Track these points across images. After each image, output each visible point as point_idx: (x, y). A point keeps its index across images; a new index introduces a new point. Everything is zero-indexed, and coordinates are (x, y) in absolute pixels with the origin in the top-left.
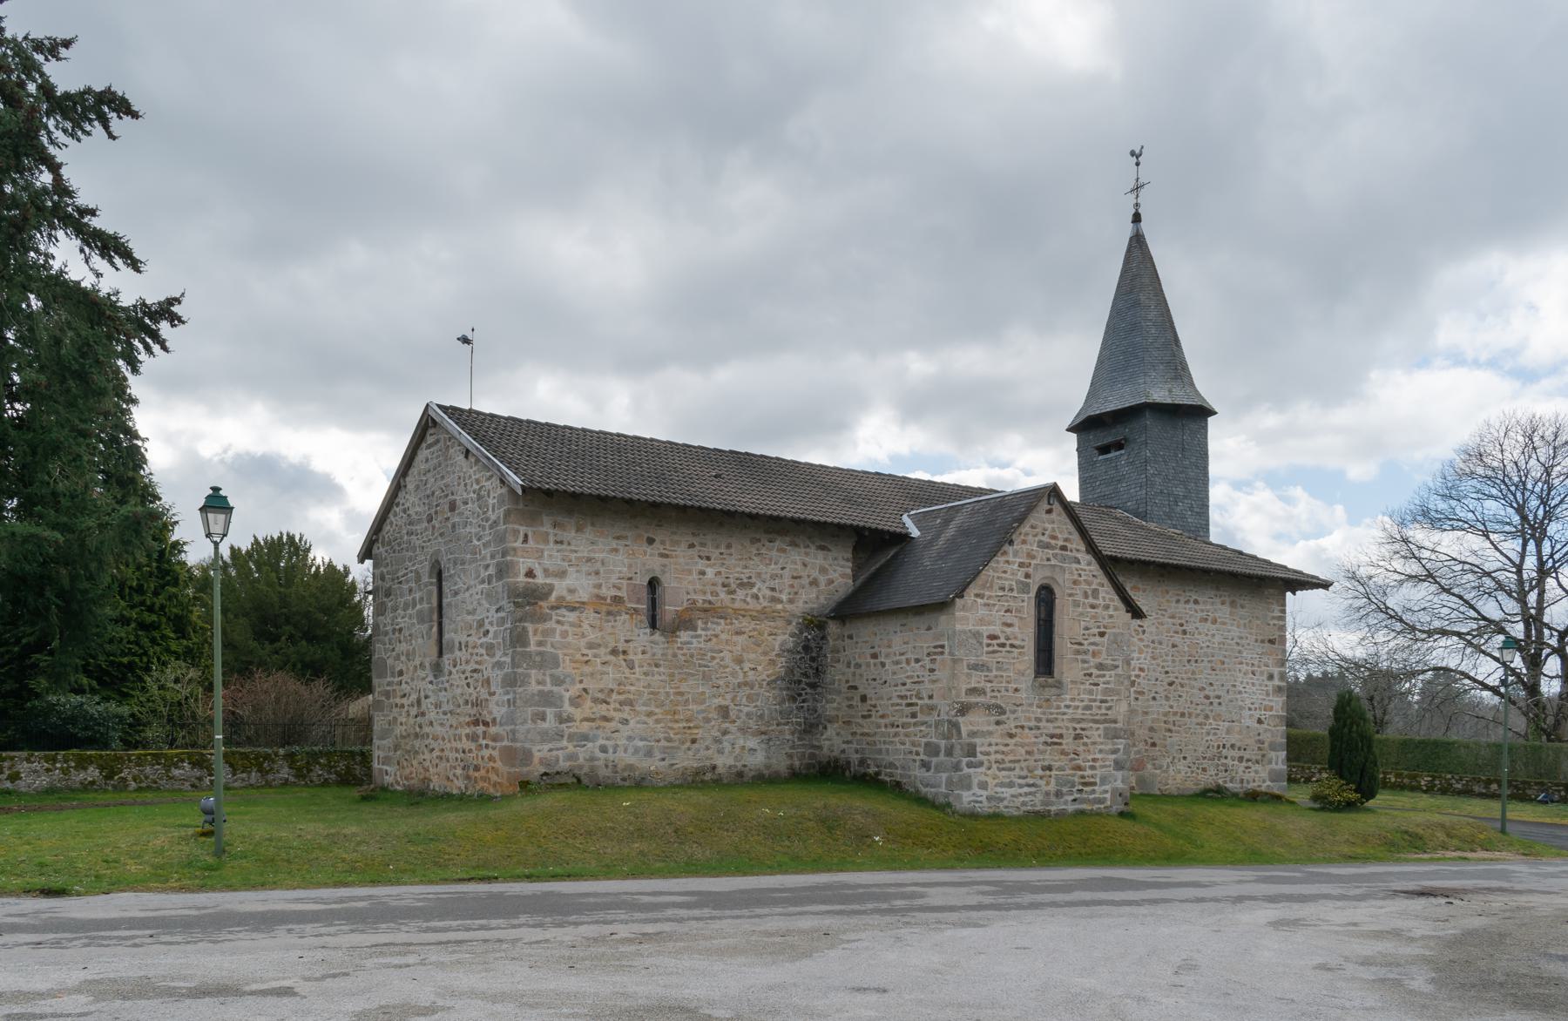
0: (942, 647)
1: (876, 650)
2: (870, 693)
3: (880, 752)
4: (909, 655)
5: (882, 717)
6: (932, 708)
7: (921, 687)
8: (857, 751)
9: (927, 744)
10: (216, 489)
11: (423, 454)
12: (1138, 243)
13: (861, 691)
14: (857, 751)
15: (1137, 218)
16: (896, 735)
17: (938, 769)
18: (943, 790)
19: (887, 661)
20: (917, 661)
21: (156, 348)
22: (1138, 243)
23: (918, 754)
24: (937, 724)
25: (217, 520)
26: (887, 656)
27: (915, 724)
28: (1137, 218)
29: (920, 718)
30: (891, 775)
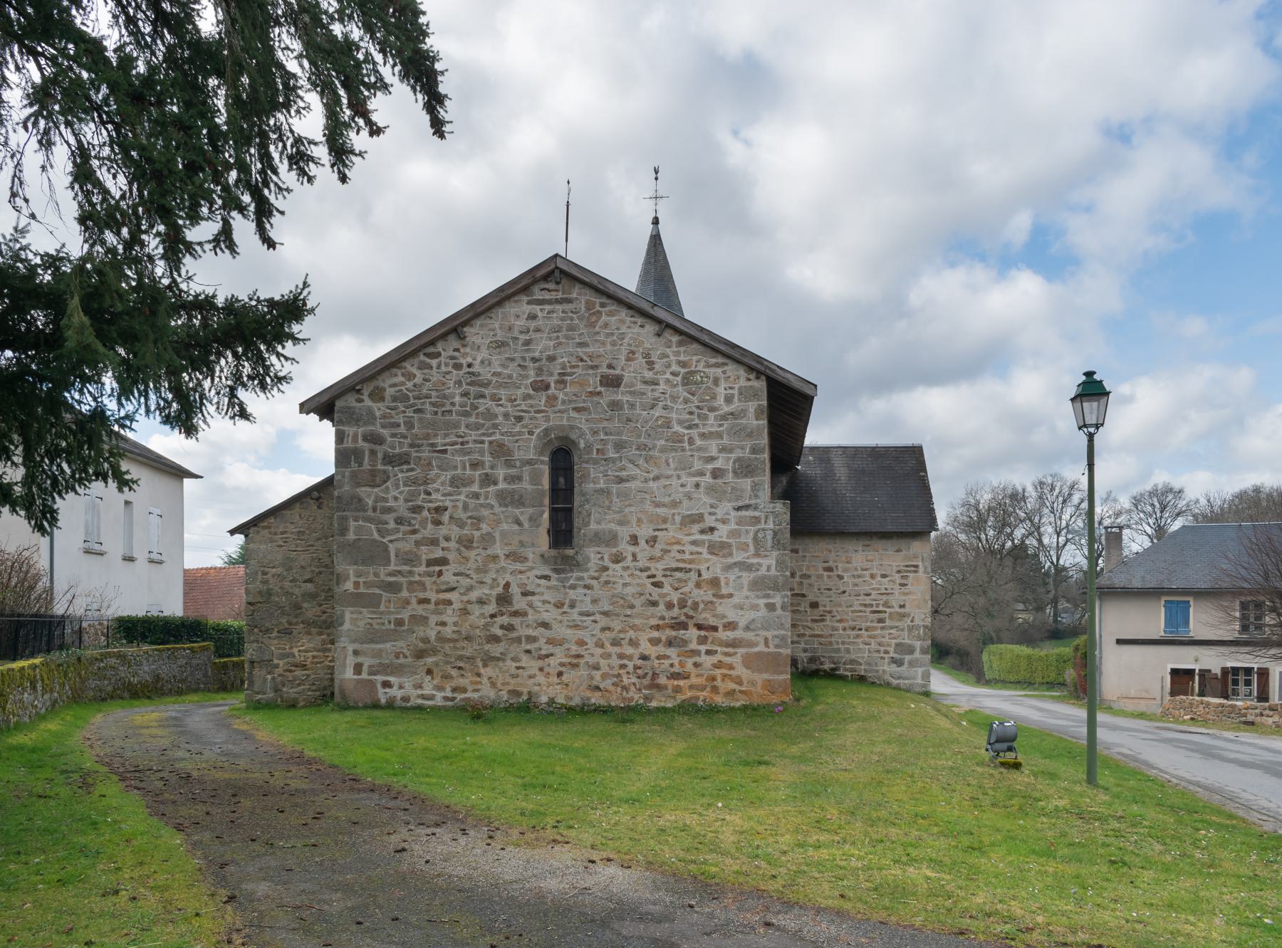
0: (916, 566)
1: (831, 564)
2: (822, 600)
3: (838, 650)
4: (875, 571)
5: (840, 621)
6: (903, 616)
7: (890, 597)
8: (805, 651)
9: (897, 645)
10: (1089, 374)
11: (519, 309)
12: (656, 240)
13: (811, 598)
14: (805, 651)
15: (656, 221)
16: (858, 636)
17: (911, 664)
18: (920, 681)
19: (845, 575)
20: (884, 576)
21: (396, 104)
22: (656, 240)
23: (886, 652)
24: (911, 629)
25: (1090, 407)
26: (845, 570)
27: (882, 628)
28: (656, 221)
29: (888, 623)
30: (852, 670)
